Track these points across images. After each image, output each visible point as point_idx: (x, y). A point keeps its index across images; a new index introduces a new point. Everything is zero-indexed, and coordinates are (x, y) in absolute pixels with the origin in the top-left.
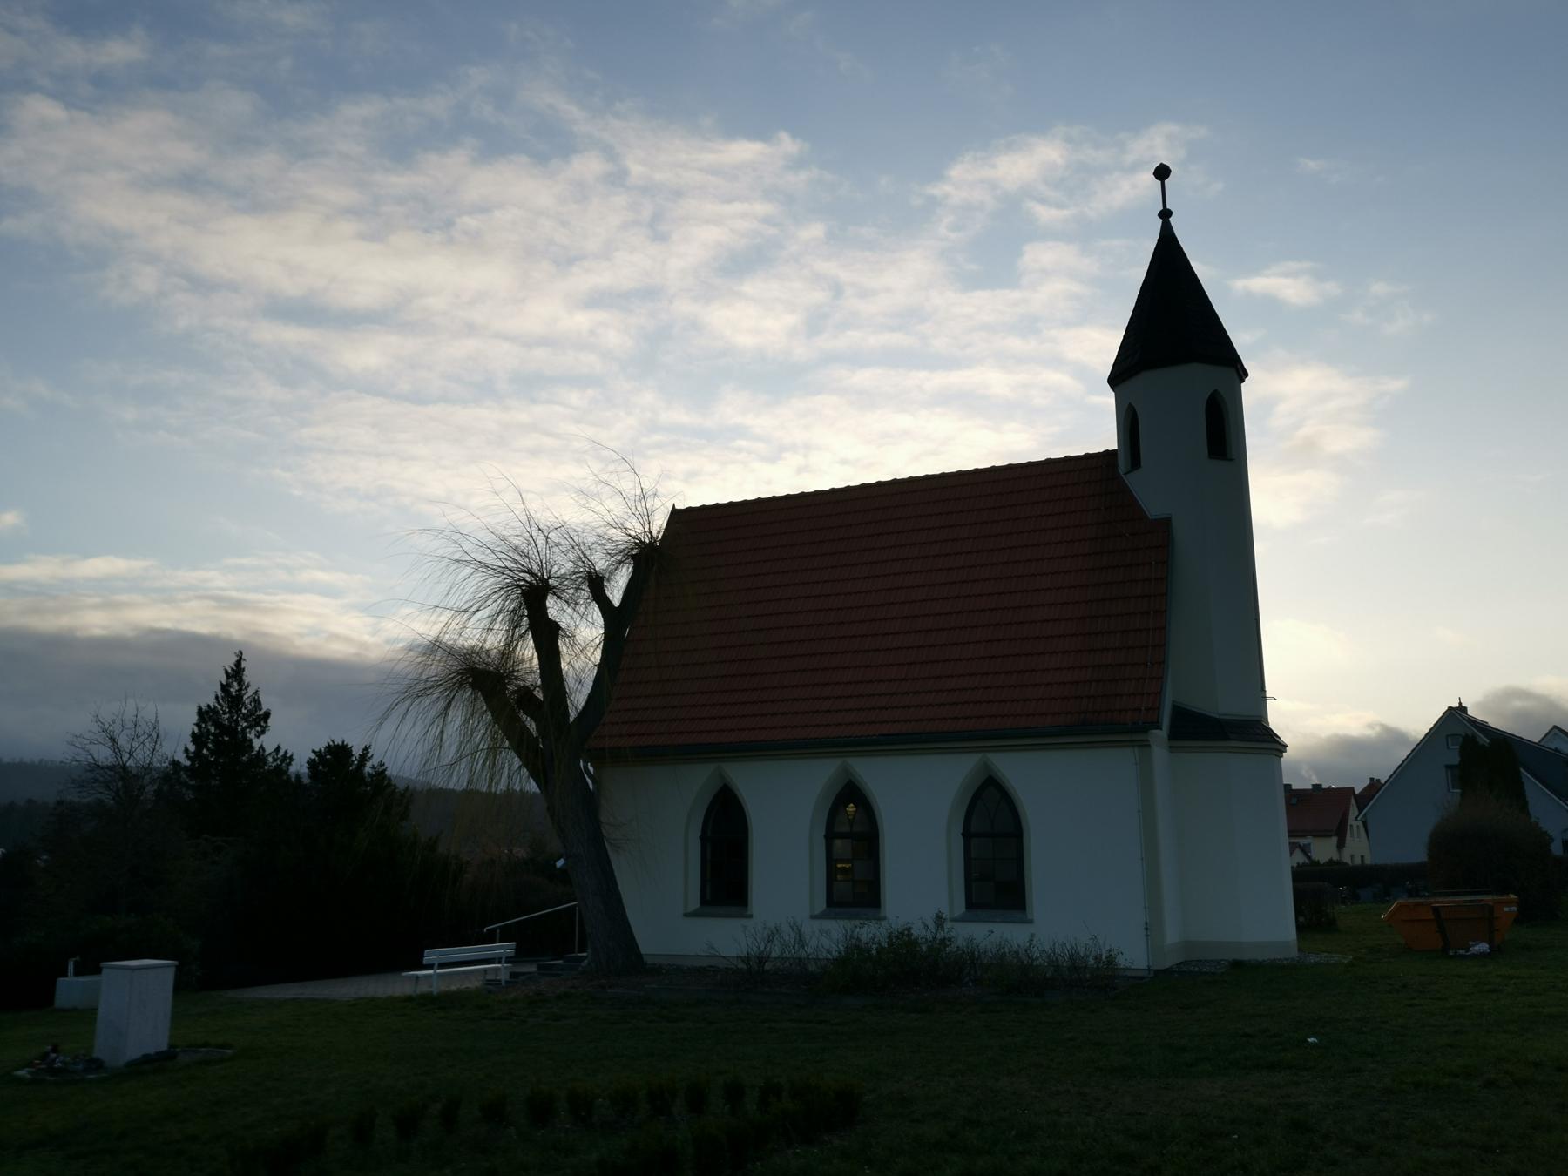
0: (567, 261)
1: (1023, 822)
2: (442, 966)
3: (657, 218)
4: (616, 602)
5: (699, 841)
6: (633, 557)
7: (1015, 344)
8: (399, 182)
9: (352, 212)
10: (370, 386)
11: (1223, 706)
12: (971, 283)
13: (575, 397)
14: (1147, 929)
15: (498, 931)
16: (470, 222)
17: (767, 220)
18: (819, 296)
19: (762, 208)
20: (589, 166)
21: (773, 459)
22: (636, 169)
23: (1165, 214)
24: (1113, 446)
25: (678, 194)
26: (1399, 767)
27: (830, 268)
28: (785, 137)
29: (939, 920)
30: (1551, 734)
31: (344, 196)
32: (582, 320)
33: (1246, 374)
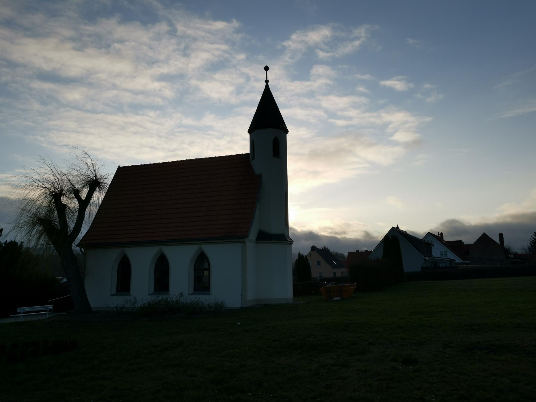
0: (152, 63)
1: (211, 267)
2: (24, 313)
3: (186, 48)
4: (83, 198)
5: (193, 270)
6: (89, 184)
7: (306, 101)
8: (90, 29)
9: (72, 39)
10: (76, 106)
11: (274, 230)
12: (294, 78)
13: (152, 114)
14: (242, 296)
15: (53, 302)
16: (117, 46)
17: (225, 51)
18: (242, 80)
19: (224, 47)
20: (163, 27)
21: (220, 138)
22: (180, 28)
23: (267, 81)
24: (249, 152)
25: (195, 39)
26: (378, 245)
27: (246, 70)
28: (234, 20)
29: (181, 295)
30: (427, 235)
31: (68, 33)
32: (156, 85)
33: (288, 131)
